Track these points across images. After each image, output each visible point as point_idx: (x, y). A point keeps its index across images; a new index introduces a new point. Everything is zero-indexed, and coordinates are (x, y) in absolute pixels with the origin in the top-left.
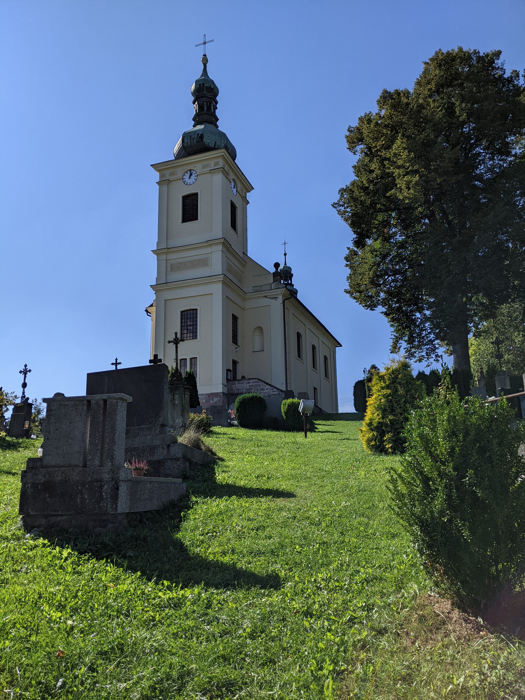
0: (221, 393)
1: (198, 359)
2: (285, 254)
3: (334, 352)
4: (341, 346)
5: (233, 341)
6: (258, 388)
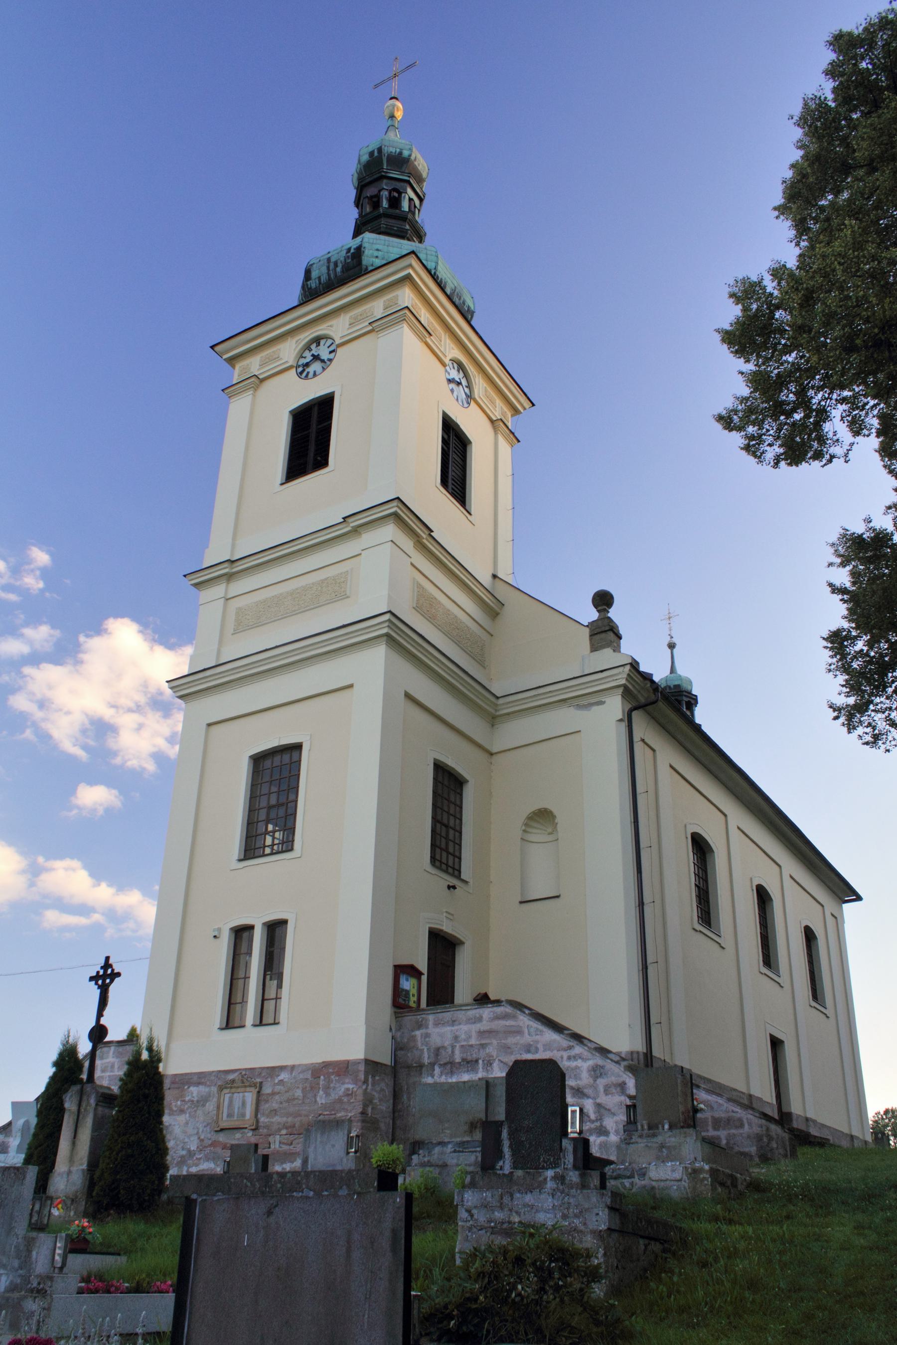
0: (356, 1063)
1: (290, 927)
2: (672, 646)
3: (838, 919)
4: (859, 898)
5: (433, 859)
6: (511, 1040)
